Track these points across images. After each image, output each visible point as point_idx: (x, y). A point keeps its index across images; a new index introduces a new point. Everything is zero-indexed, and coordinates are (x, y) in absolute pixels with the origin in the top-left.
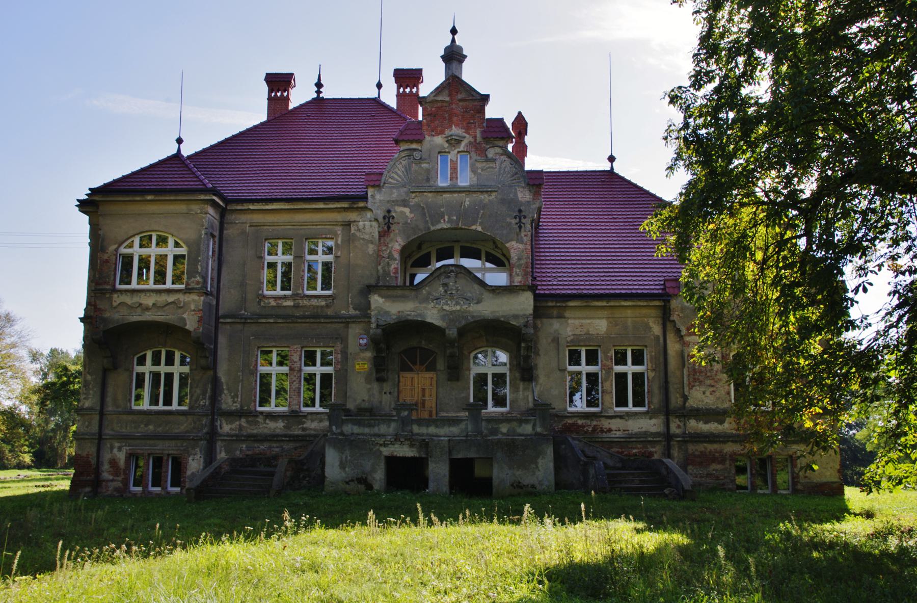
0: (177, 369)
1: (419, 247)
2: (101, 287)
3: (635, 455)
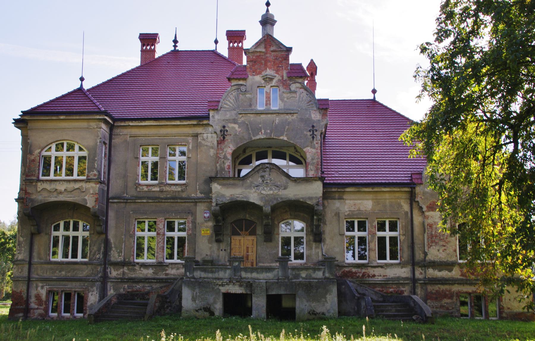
0: (81, 234)
1: (244, 151)
2: (29, 178)
3: (391, 292)
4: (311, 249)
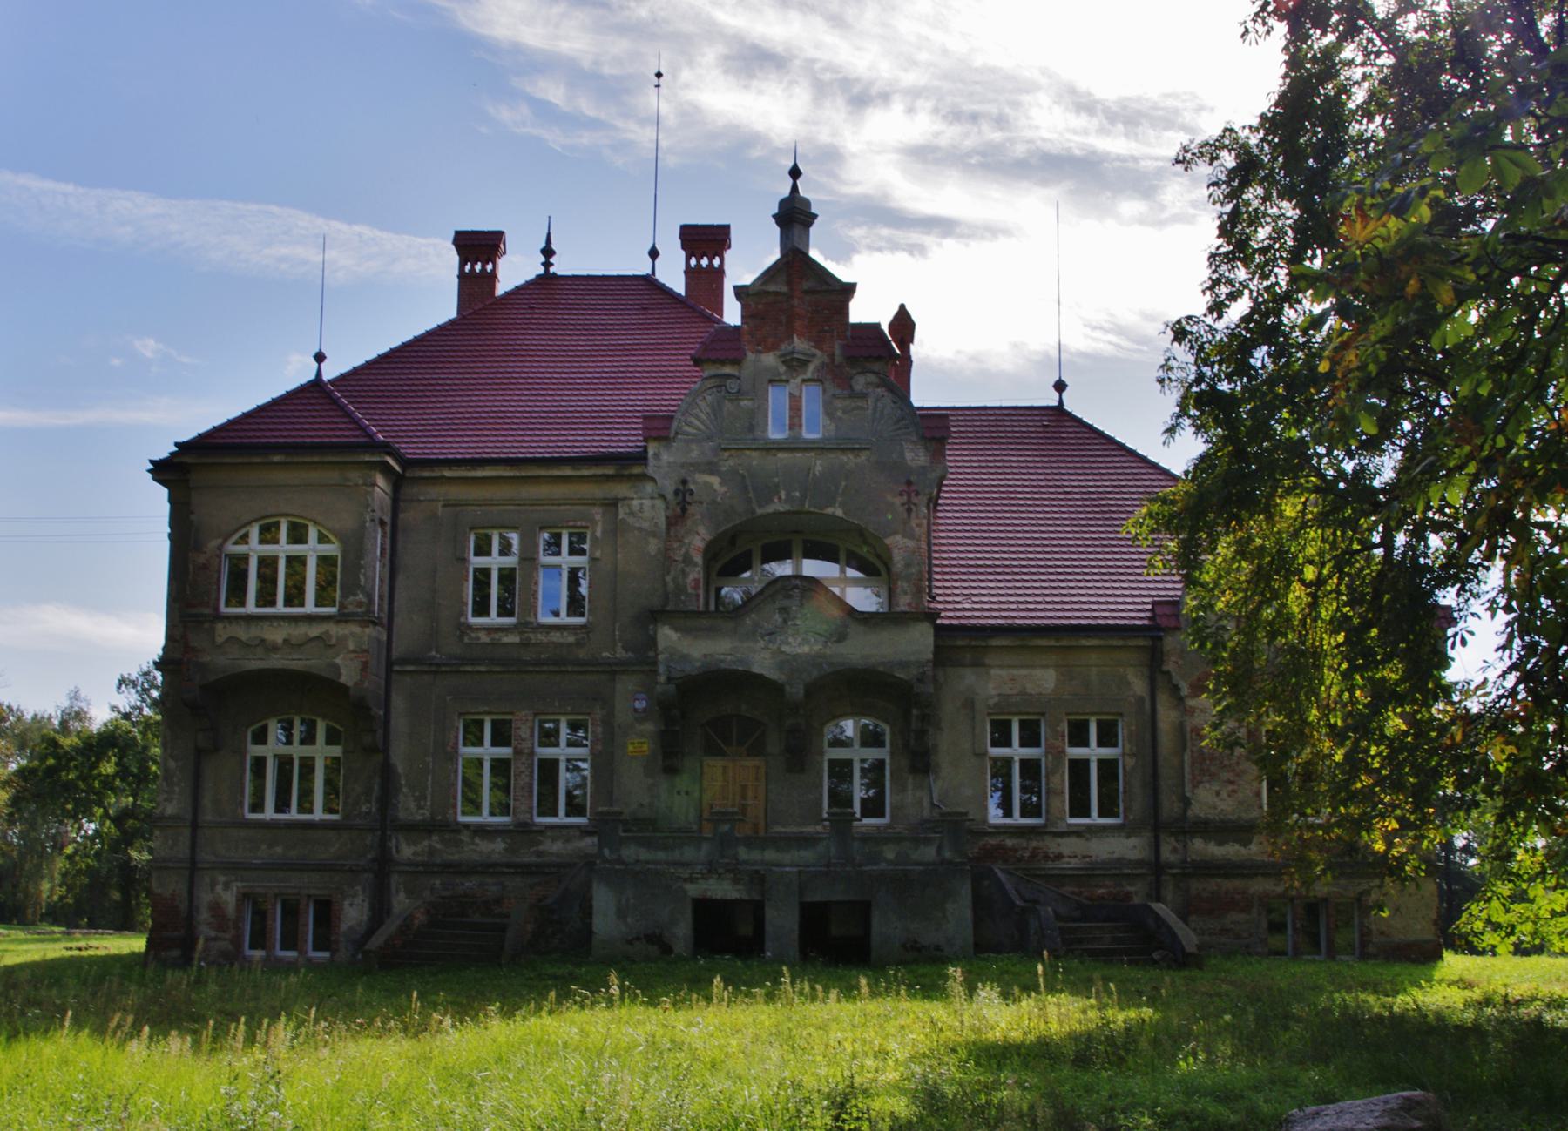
2: (194, 611)
3: (1102, 897)
4: (904, 790)
